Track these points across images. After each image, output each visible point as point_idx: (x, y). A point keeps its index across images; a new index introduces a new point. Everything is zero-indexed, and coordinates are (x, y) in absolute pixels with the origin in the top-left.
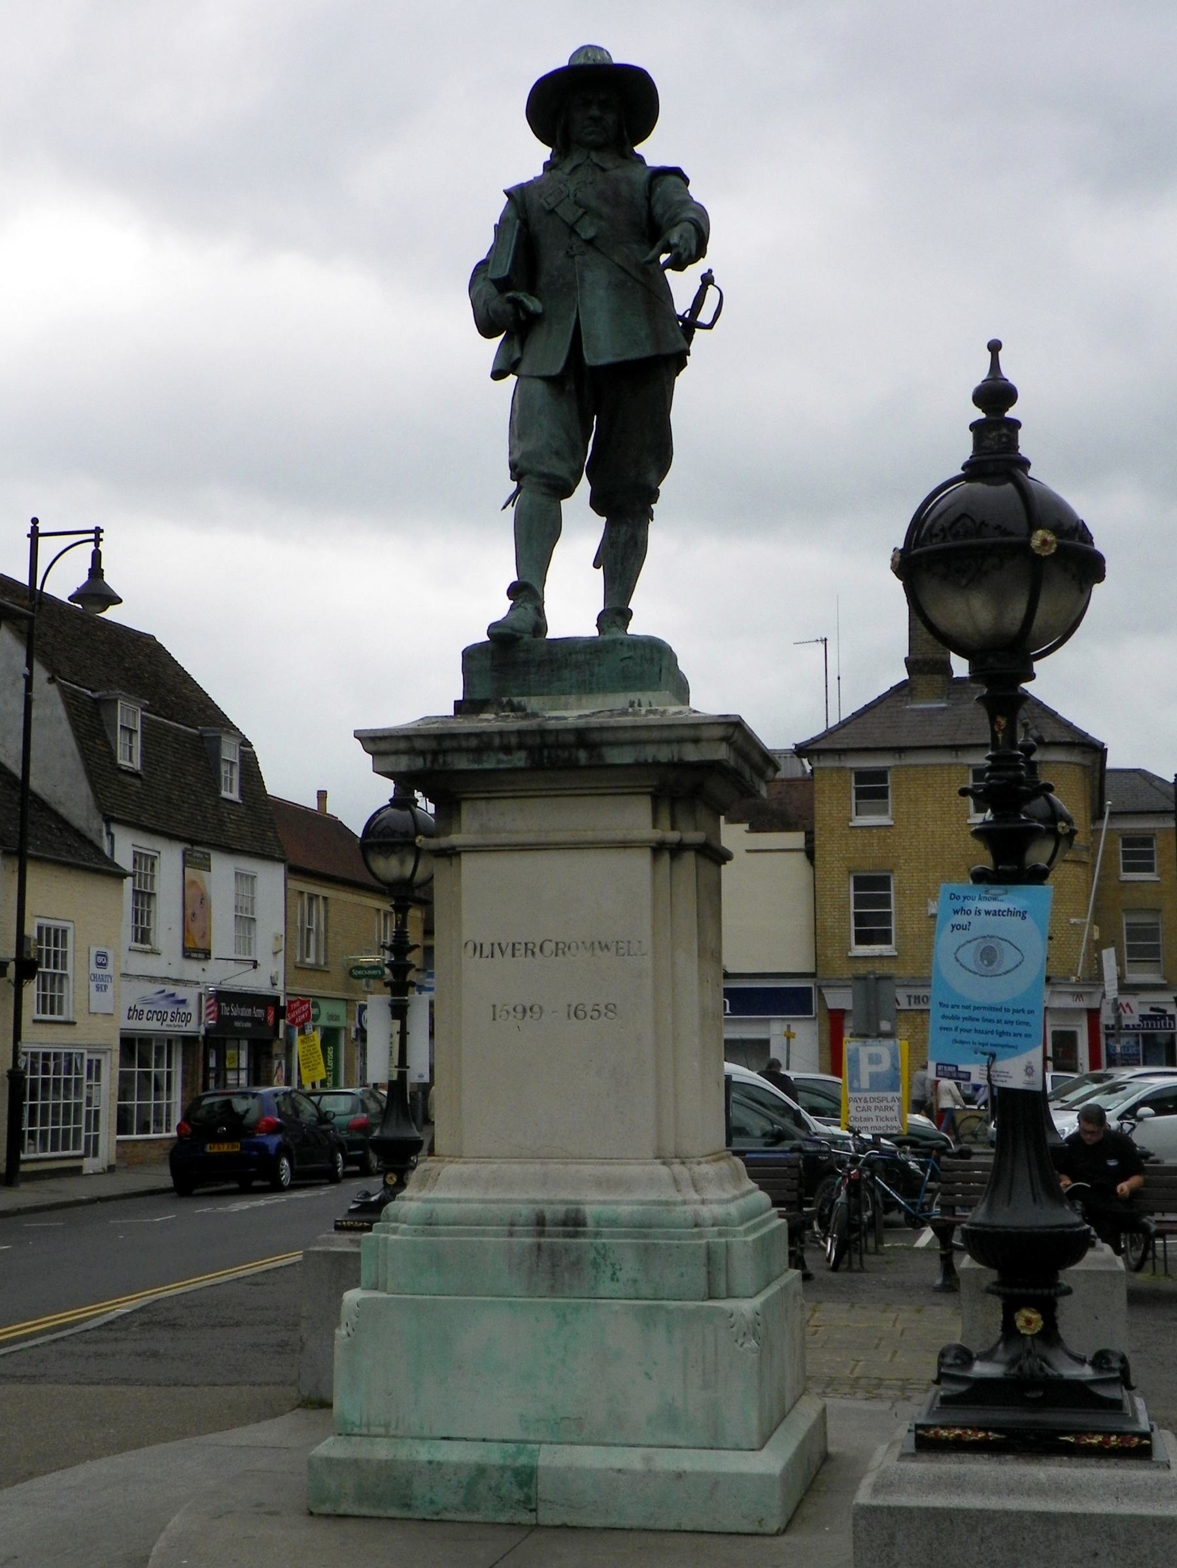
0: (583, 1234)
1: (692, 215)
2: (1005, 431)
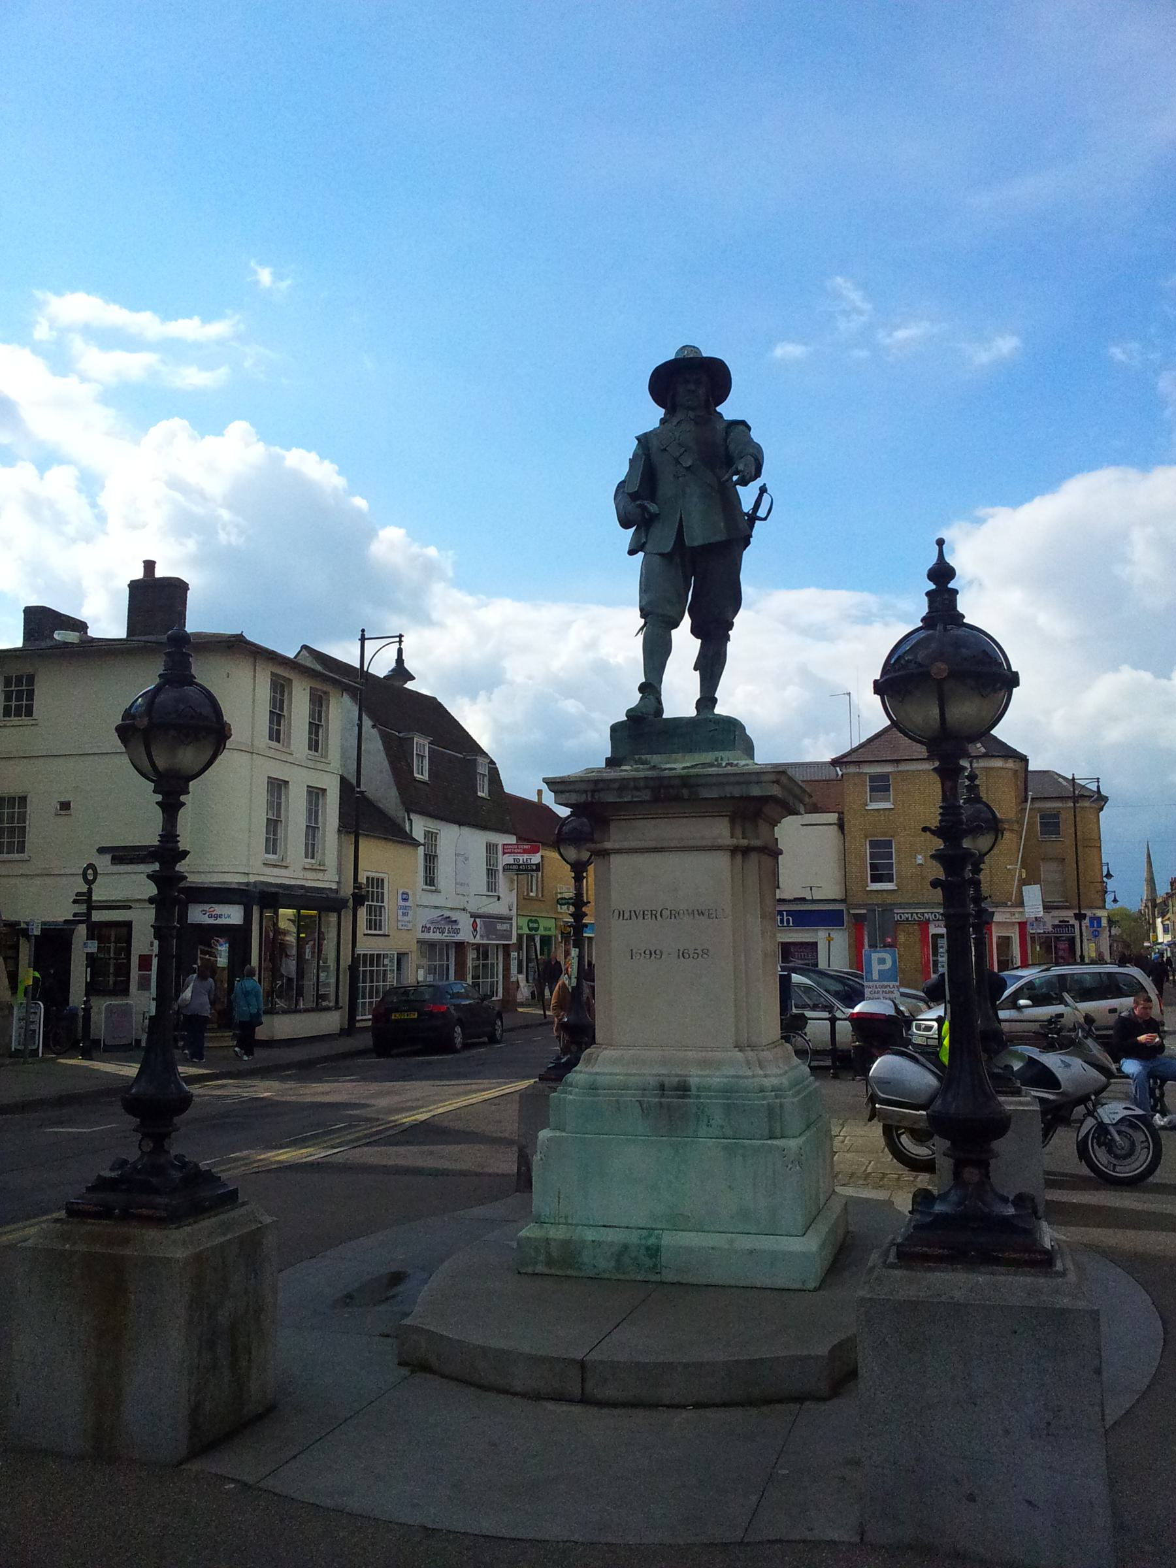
0: (689, 1097)
1: (751, 450)
2: (946, 596)
